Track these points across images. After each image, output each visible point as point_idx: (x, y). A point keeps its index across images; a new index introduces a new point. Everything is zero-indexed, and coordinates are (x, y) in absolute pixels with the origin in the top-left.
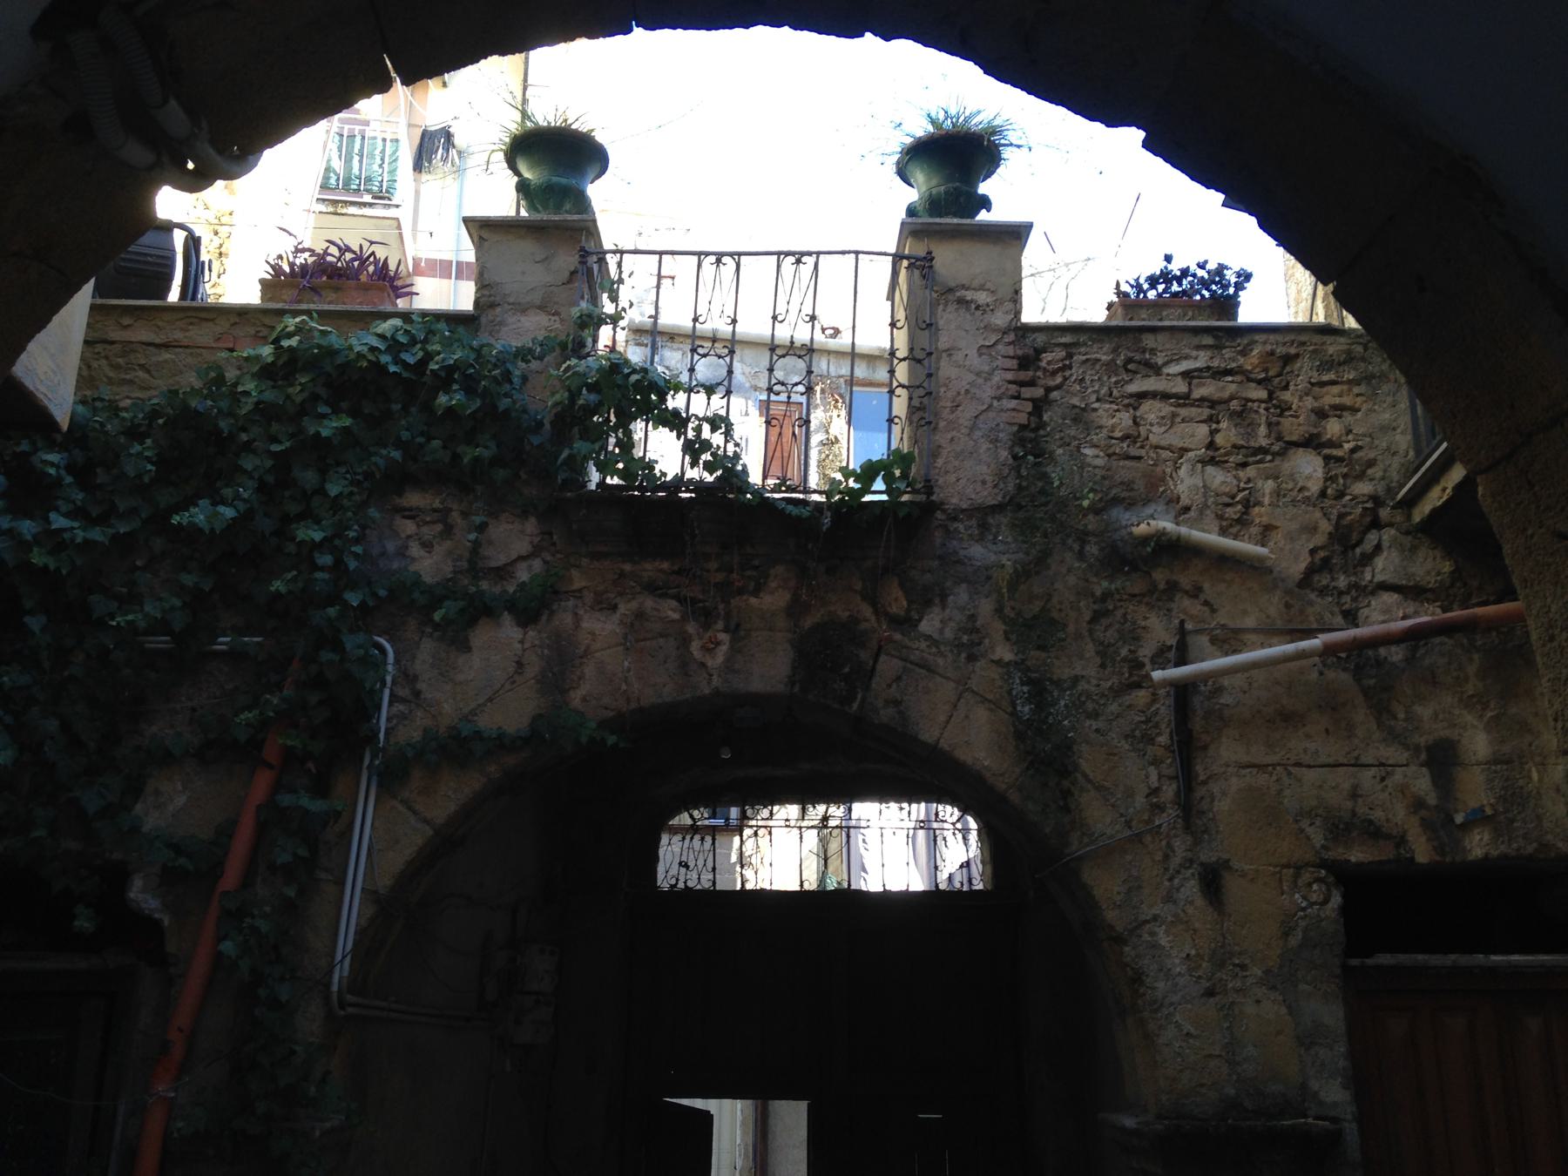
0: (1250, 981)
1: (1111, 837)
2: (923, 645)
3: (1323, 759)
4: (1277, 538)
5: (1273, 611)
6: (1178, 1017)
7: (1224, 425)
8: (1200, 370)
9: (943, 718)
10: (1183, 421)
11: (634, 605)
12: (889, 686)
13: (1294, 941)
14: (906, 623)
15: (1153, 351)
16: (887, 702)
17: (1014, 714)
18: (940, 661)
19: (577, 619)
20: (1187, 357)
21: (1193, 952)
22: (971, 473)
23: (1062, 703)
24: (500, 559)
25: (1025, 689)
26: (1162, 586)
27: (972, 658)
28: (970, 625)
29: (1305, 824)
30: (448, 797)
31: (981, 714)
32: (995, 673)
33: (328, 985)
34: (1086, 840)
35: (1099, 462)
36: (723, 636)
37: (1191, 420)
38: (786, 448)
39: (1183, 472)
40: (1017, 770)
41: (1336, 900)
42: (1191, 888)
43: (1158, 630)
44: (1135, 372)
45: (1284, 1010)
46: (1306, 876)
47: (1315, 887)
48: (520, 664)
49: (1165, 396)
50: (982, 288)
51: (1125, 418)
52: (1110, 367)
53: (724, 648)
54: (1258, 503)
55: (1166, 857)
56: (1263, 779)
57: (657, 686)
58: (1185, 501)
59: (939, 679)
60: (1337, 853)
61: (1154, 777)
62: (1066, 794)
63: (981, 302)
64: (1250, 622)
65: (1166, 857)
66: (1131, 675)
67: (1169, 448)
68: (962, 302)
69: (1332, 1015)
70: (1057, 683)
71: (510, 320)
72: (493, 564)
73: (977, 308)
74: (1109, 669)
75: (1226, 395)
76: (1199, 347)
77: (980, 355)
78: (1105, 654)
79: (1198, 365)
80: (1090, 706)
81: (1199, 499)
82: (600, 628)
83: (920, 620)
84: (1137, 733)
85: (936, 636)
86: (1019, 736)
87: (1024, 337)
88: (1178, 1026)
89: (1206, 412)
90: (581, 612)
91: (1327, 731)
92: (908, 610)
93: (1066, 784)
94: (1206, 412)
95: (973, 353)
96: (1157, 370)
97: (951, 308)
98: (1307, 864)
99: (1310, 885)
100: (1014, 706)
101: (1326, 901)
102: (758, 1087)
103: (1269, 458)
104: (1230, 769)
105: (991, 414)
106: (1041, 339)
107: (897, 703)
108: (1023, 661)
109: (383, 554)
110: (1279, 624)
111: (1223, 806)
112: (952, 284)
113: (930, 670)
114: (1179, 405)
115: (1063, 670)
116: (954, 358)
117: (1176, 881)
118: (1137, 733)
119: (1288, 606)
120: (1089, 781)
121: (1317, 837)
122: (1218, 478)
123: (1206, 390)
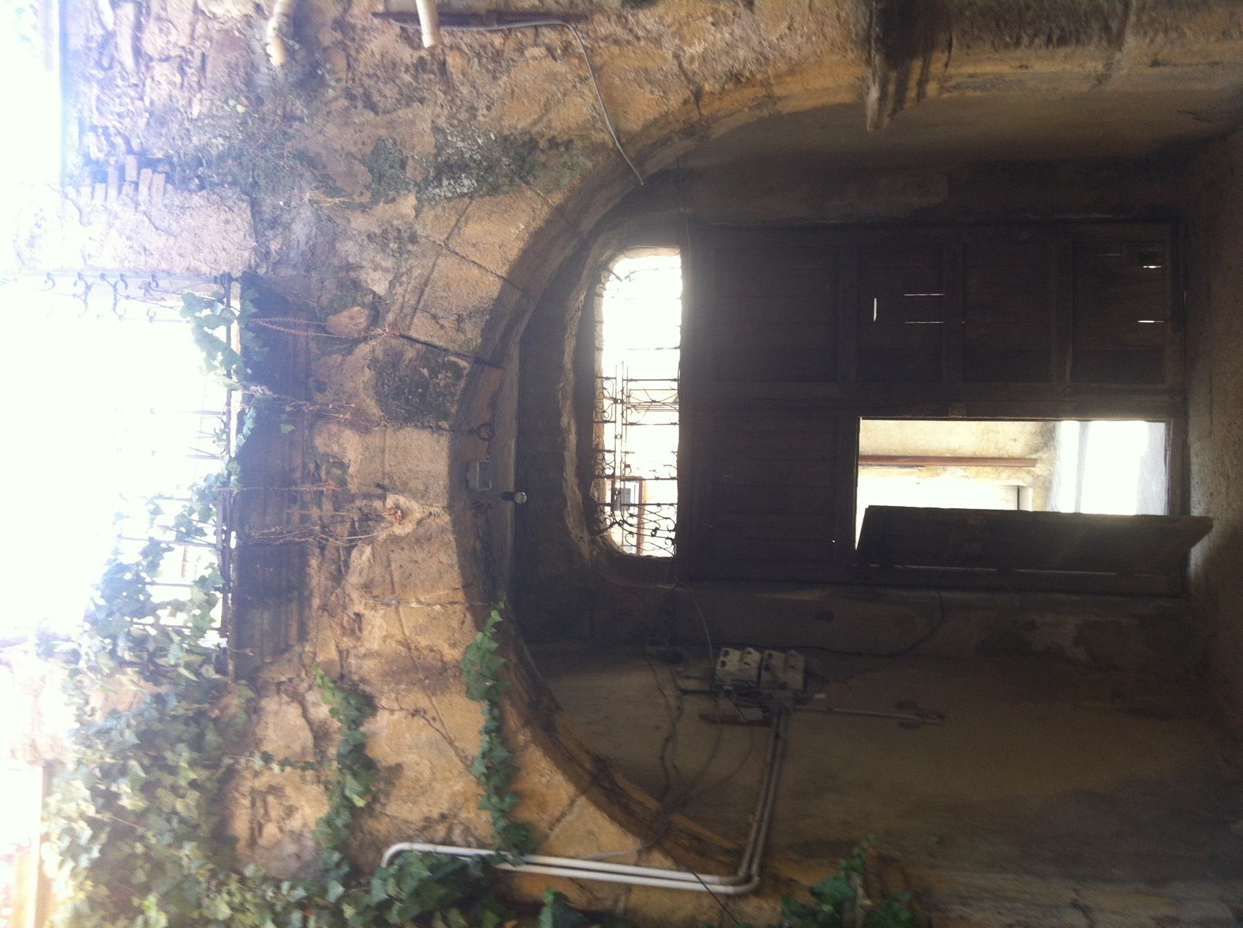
2: (399, 290)
6: (773, 38)
9: (476, 271)
10: (165, 9)
12: (442, 327)
14: (376, 310)
18: (417, 272)
19: (369, 655)
21: (710, 19)
23: (460, 144)
25: (445, 182)
26: (339, 35)
27: (413, 239)
31: (472, 230)
32: (429, 214)
33: (728, 896)
36: (390, 502)
40: (529, 194)
48: (415, 713)
49: (138, 27)
53: (402, 500)
55: (616, 42)
62: (553, 143)
66: (432, 72)
67: (193, 26)
70: (440, 149)
73: (39, 226)
74: (426, 94)
78: (409, 98)
83: (374, 293)
85: (390, 277)
86: (494, 190)
88: (781, 38)
90: (362, 650)
92: (363, 305)
96: (109, 36)
100: (463, 195)
102: (845, 461)
105: (154, 213)
107: (460, 319)
108: (416, 184)
109: (298, 856)
117: (640, 33)
120: (540, 118)
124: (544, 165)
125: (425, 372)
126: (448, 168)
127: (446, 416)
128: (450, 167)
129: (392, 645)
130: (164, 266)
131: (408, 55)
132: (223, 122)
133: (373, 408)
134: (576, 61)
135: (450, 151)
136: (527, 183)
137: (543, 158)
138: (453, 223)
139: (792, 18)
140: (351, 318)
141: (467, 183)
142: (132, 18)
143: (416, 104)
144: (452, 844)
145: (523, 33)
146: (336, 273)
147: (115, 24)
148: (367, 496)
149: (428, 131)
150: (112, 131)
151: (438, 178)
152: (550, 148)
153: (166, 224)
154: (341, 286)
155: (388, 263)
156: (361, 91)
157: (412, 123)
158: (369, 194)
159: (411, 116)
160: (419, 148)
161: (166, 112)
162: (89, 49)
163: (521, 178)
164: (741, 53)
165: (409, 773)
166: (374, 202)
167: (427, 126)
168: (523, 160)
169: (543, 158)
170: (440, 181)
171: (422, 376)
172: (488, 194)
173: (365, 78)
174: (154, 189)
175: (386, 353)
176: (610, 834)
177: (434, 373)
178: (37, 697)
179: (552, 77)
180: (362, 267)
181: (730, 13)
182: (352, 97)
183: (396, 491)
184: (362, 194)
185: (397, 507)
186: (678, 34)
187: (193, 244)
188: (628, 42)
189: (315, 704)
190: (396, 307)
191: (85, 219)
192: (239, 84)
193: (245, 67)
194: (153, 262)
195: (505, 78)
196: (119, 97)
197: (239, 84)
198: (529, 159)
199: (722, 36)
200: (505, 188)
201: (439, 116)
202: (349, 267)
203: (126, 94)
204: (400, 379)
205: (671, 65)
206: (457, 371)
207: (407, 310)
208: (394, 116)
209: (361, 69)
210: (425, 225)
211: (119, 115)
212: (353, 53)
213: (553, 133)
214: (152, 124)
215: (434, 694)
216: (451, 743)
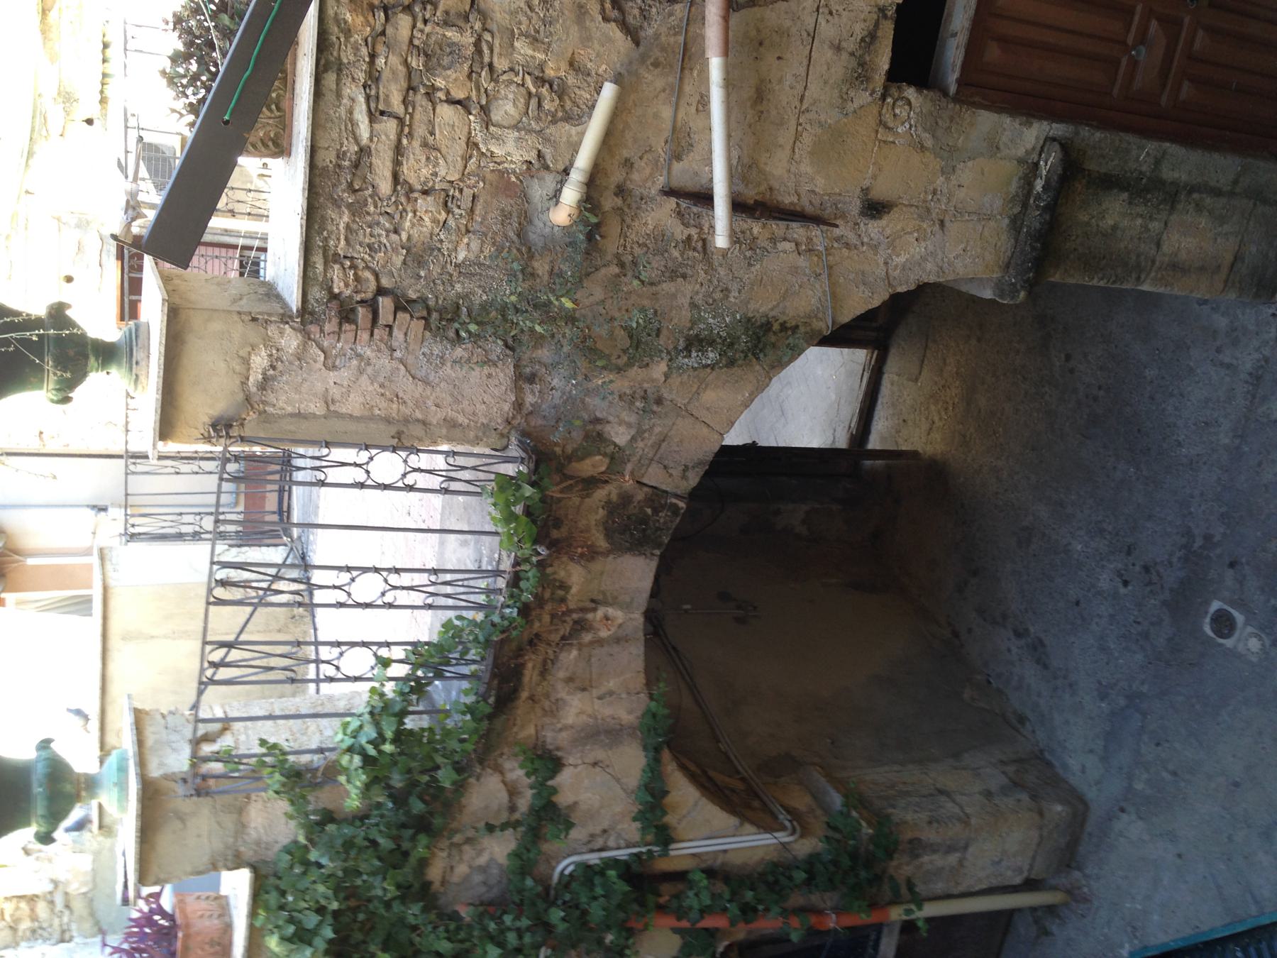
2: (641, 444)
9: (705, 430)
10: (432, 133)
12: (671, 475)
14: (617, 458)
18: (657, 430)
23: (711, 321)
25: (694, 354)
26: (619, 202)
27: (659, 401)
31: (709, 396)
32: (675, 380)
35: (475, 245)
40: (758, 367)
48: (595, 764)
49: (398, 150)
50: (246, 362)
55: (847, 245)
62: (784, 327)
66: (695, 249)
70: (693, 323)
73: (273, 367)
74: (689, 272)
78: (674, 274)
83: (616, 445)
85: (633, 432)
86: (731, 363)
88: (956, 257)
90: (559, 726)
93: (776, 327)
96: (364, 151)
105: (410, 360)
106: (316, 293)
107: (686, 468)
108: (668, 353)
109: (484, 883)
117: (865, 240)
124: (774, 345)
125: (649, 511)
126: (696, 343)
127: (658, 546)
128: (701, 341)
130: (419, 415)
132: (491, 273)
133: (602, 543)
134: (815, 259)
135: (702, 326)
136: (758, 359)
137: (773, 339)
138: (694, 389)
140: (593, 466)
141: (712, 355)
142: (393, 137)
143: (680, 280)
145: (778, 227)
146: (585, 425)
148: (583, 610)
149: (686, 305)
150: (361, 265)
151: (688, 348)
152: (781, 331)
153: (423, 373)
154: (587, 437)
155: (633, 419)
156: (630, 258)
157: (674, 296)
158: (625, 358)
161: (424, 251)
163: (754, 354)
164: (929, 266)
166: (629, 365)
167: (685, 301)
169: (773, 339)
170: (690, 351)
171: (645, 513)
173: (635, 246)
177: (656, 511)
179: (795, 270)
182: (622, 265)
184: (619, 357)
185: (607, 618)
186: (891, 245)
187: (452, 395)
189: (512, 770)
190: (635, 459)
191: (330, 362)
192: (511, 234)
193: (519, 217)
194: (406, 411)
196: (370, 227)
197: (511, 234)
199: (917, 250)
200: (740, 362)
201: (697, 293)
202: (598, 421)
203: (378, 224)
204: (629, 518)
205: (881, 271)
206: (675, 509)
209: (633, 236)
210: (671, 390)
211: (370, 246)
212: (628, 220)
213: (785, 318)
216: (618, 780)
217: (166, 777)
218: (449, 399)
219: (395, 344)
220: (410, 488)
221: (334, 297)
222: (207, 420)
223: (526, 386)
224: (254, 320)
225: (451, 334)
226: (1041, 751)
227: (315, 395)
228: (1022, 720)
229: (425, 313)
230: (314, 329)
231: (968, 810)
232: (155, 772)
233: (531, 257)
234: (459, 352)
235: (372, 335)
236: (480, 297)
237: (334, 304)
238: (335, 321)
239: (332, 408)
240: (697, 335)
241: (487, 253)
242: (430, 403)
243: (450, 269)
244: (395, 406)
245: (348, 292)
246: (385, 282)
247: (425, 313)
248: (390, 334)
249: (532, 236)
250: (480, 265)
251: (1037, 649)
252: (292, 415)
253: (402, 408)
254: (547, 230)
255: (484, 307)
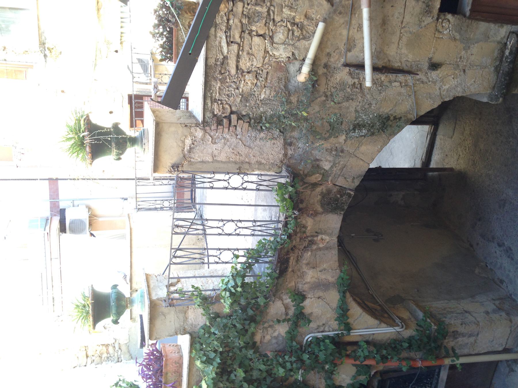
0: (465, 57)
1: (413, 103)
2: (335, 169)
3: (402, 11)
4: (312, 13)
5: (342, 21)
6: (469, 84)
7: (254, 28)
8: (226, 37)
9: (362, 162)
10: (251, 49)
11: (304, 266)
12: (347, 181)
13: (458, 37)
14: (325, 175)
15: (217, 60)
16: (353, 182)
17: (364, 136)
18: (342, 163)
19: (306, 283)
20: (220, 43)
21: (453, 76)
22: (271, 149)
23: (364, 117)
24: (283, 309)
25: (357, 131)
26: (325, 70)
27: (342, 151)
28: (329, 151)
29: (423, 24)
30: (356, 310)
31: (363, 148)
32: (349, 142)
34: (411, 112)
35: (268, 92)
37: (251, 45)
38: (264, 228)
39: (277, 54)
40: (384, 136)
41: (449, 16)
42: (434, 75)
43: (342, 75)
44: (225, 69)
45: (476, 45)
46: (440, 28)
47: (444, 25)
48: (319, 298)
49: (238, 56)
50: (183, 142)
51: (248, 77)
52: (223, 81)
53: (324, 236)
54: (294, 18)
55: (423, 82)
56: (404, 39)
57: (333, 255)
58: (290, 55)
59: (348, 164)
60: (436, 11)
61: (397, 84)
62: (395, 118)
63: (190, 142)
64: (345, 32)
65: (423, 82)
66: (357, 88)
67: (264, 58)
68: (190, 150)
69: (483, 26)
70: (356, 118)
71: (190, 322)
72: (284, 311)
73: (193, 144)
74: (355, 97)
75: (239, 24)
76: (216, 36)
77: (215, 143)
78: (348, 99)
79: (224, 37)
80: (367, 106)
81: (290, 48)
82: (311, 276)
83: (324, 169)
84: (380, 88)
85: (332, 164)
86: (373, 134)
87: (207, 122)
88: (471, 85)
89: (246, 35)
90: (304, 282)
91: (392, 6)
92: (320, 174)
93: (392, 118)
94: (246, 35)
95: (215, 146)
96: (225, 58)
97: (192, 155)
98: (436, 26)
99: (443, 26)
100: (362, 136)
101: (449, 21)
103: (272, 8)
104: (398, 52)
105: (244, 139)
106: (208, 115)
107: (354, 178)
108: (346, 131)
109: (277, 343)
110: (347, 19)
111: (410, 57)
112: (182, 155)
113: (345, 166)
114: (243, 50)
115: (351, 116)
116: (217, 154)
117: (430, 79)
118: (380, 88)
119: (340, 13)
120: (392, 109)
121: (428, 20)
122: (280, 36)
123: (236, 35)
124: (391, 126)
127: (343, 210)
129: (314, 279)
130: (247, 160)
131: (350, 81)
132: (274, 103)
135: (360, 119)
136: (384, 132)
139: (476, 78)
141: (364, 131)
142: (236, 51)
144: (326, 332)
145: (392, 76)
147: (228, 53)
148: (312, 236)
149: (353, 111)
151: (354, 129)
152: (394, 120)
153: (248, 144)
155: (331, 159)
156: (330, 93)
158: (328, 134)
159: (348, 105)
160: (349, 118)
161: (248, 96)
162: (216, 64)
163: (382, 130)
165: (315, 314)
166: (330, 137)
168: (384, 124)
172: (371, 135)
173: (332, 88)
174: (244, 129)
175: (326, 190)
176: (371, 321)
177: (341, 196)
178: (185, 313)
179: (400, 94)
180: (321, 160)
181: (458, 74)
182: (326, 96)
183: (322, 234)
188: (426, 83)
189: (286, 299)
191: (214, 141)
192: (282, 87)
195: (384, 93)
197: (282, 87)
198: (386, 124)
200: (376, 134)
201: (358, 106)
203: (231, 86)
205: (437, 92)
207: (337, 176)
208: (342, 105)
209: (331, 84)
213: (396, 114)
214: (243, 101)
215: (325, 292)
217: (158, 299)
218: (259, 153)
219: (238, 133)
220: (245, 189)
221: (215, 116)
222: (170, 165)
223: (289, 147)
224: (186, 126)
225: (259, 128)
226: (511, 295)
227: (208, 154)
228: (502, 282)
229: (249, 120)
230: (207, 128)
231: (479, 319)
232: (154, 297)
233: (290, 95)
234: (262, 135)
235: (229, 130)
236: (270, 112)
237: (215, 119)
238: (215, 125)
239: (215, 159)
240: (358, 123)
241: (272, 95)
242: (251, 155)
243: (258, 102)
244: (238, 157)
245: (220, 114)
246: (234, 109)
247: (249, 120)
248: (236, 129)
249: (290, 87)
250: (270, 100)
251: (508, 252)
252: (200, 162)
253: (241, 158)
254: (296, 84)
255: (272, 116)
